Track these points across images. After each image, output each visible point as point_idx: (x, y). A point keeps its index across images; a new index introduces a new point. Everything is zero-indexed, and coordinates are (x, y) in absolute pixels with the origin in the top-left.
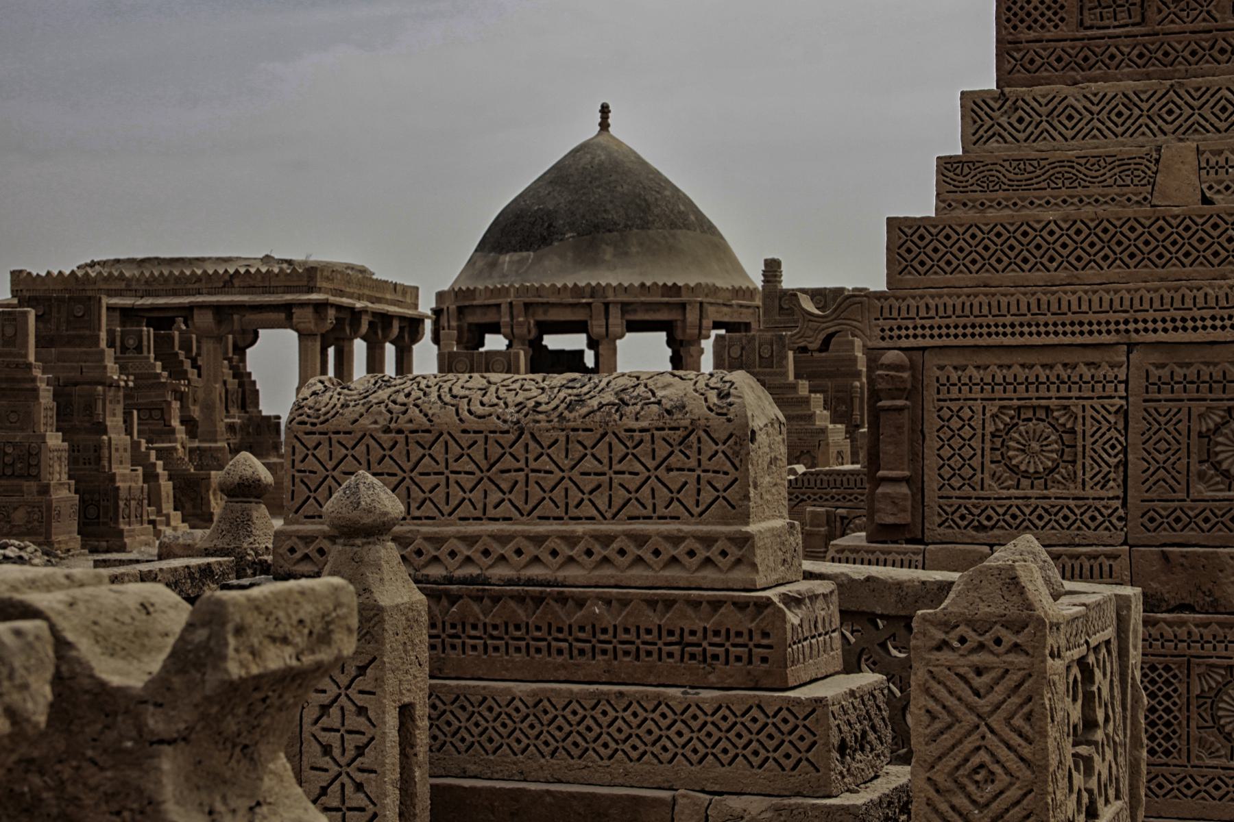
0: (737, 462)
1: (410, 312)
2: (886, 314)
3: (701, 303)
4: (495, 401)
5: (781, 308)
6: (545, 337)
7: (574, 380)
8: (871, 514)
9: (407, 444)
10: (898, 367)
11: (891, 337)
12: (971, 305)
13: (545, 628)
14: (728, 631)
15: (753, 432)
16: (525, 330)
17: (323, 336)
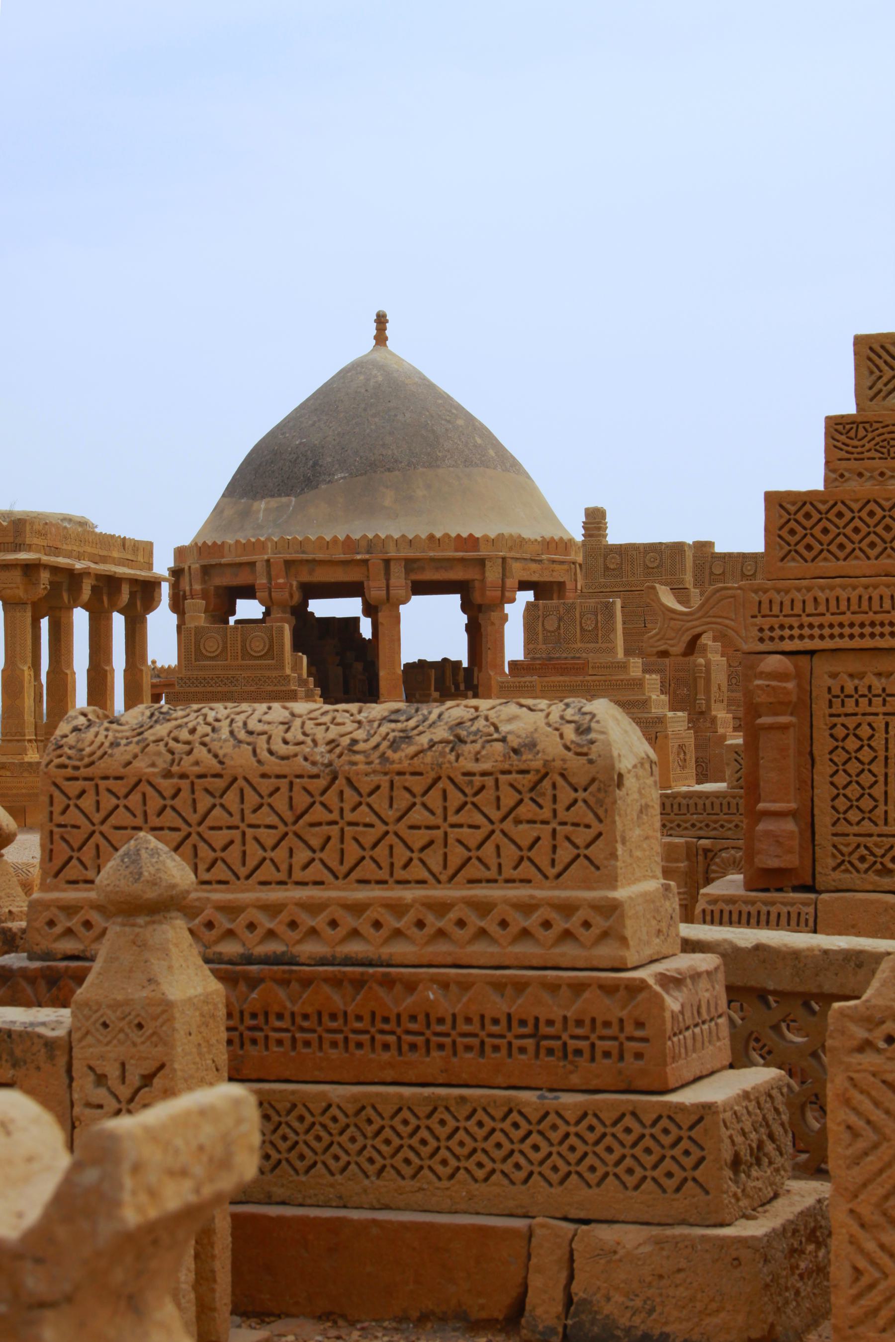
0: (601, 812)
1: (142, 574)
2: (765, 610)
3: (504, 559)
4: (301, 738)
5: (607, 568)
6: (311, 602)
7: (397, 711)
8: (750, 853)
9: (193, 792)
10: (782, 676)
11: (772, 639)
12: (870, 598)
13: (367, 1018)
14: (593, 1020)
15: (620, 776)
16: (287, 595)
17: (34, 605)
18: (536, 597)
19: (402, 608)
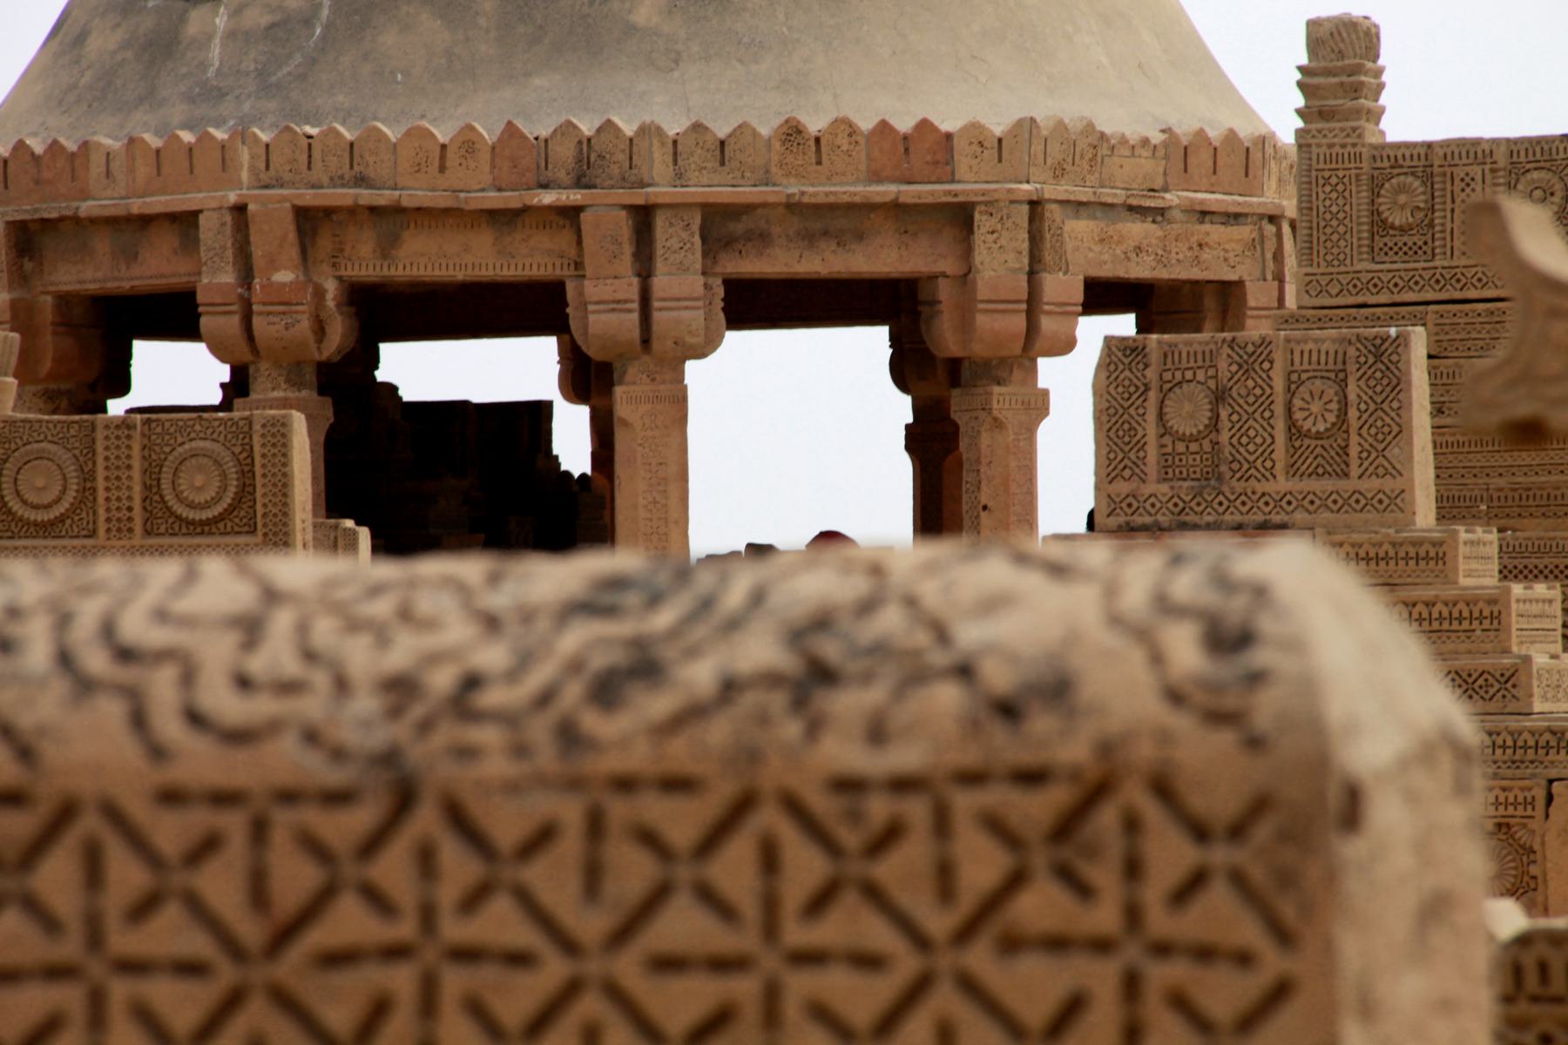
0: (1288, 911)
4: (291, 666)
5: (1379, 224)
6: (386, 349)
16: (304, 325)
18: (1142, 327)
19: (694, 371)
